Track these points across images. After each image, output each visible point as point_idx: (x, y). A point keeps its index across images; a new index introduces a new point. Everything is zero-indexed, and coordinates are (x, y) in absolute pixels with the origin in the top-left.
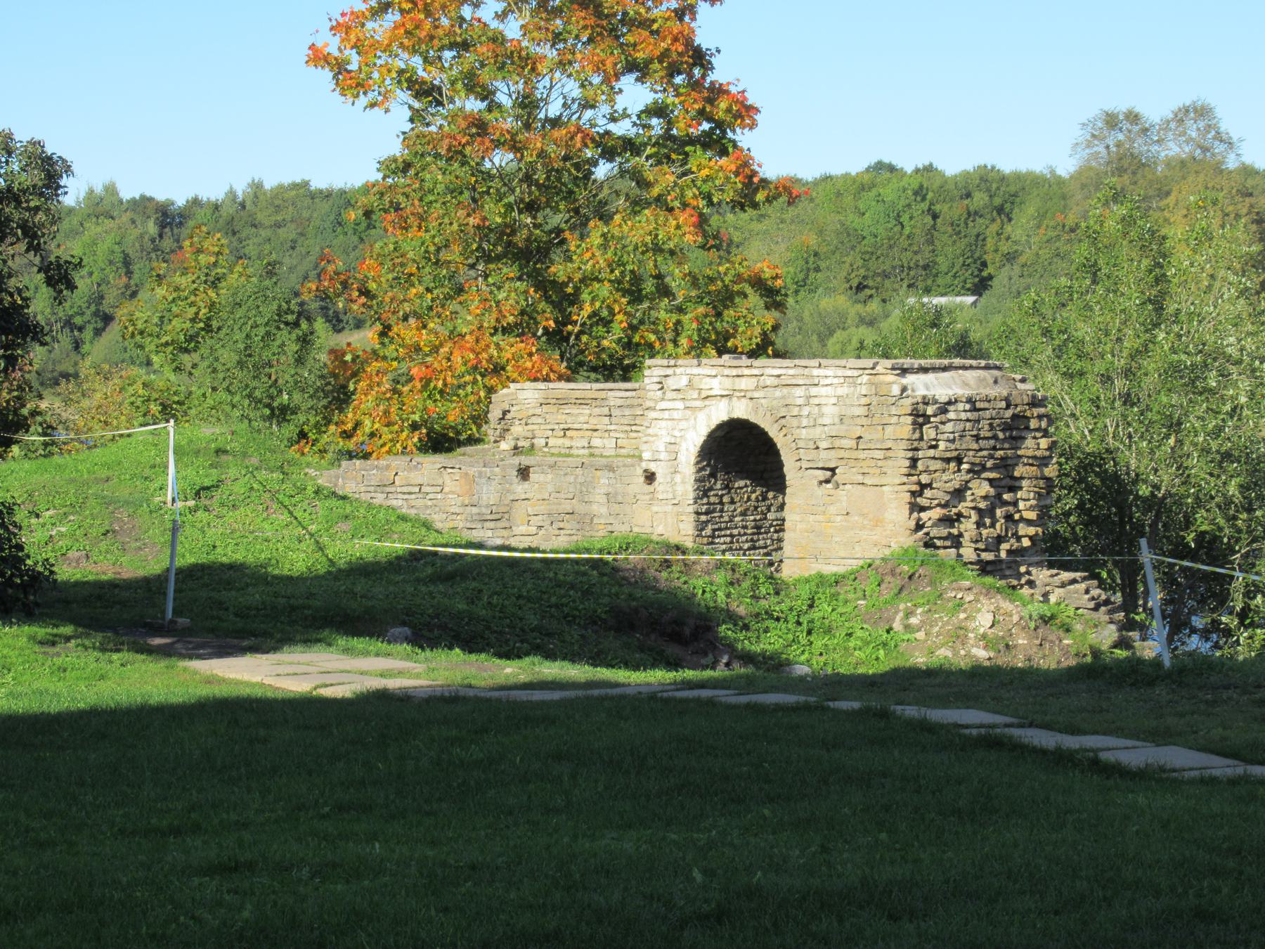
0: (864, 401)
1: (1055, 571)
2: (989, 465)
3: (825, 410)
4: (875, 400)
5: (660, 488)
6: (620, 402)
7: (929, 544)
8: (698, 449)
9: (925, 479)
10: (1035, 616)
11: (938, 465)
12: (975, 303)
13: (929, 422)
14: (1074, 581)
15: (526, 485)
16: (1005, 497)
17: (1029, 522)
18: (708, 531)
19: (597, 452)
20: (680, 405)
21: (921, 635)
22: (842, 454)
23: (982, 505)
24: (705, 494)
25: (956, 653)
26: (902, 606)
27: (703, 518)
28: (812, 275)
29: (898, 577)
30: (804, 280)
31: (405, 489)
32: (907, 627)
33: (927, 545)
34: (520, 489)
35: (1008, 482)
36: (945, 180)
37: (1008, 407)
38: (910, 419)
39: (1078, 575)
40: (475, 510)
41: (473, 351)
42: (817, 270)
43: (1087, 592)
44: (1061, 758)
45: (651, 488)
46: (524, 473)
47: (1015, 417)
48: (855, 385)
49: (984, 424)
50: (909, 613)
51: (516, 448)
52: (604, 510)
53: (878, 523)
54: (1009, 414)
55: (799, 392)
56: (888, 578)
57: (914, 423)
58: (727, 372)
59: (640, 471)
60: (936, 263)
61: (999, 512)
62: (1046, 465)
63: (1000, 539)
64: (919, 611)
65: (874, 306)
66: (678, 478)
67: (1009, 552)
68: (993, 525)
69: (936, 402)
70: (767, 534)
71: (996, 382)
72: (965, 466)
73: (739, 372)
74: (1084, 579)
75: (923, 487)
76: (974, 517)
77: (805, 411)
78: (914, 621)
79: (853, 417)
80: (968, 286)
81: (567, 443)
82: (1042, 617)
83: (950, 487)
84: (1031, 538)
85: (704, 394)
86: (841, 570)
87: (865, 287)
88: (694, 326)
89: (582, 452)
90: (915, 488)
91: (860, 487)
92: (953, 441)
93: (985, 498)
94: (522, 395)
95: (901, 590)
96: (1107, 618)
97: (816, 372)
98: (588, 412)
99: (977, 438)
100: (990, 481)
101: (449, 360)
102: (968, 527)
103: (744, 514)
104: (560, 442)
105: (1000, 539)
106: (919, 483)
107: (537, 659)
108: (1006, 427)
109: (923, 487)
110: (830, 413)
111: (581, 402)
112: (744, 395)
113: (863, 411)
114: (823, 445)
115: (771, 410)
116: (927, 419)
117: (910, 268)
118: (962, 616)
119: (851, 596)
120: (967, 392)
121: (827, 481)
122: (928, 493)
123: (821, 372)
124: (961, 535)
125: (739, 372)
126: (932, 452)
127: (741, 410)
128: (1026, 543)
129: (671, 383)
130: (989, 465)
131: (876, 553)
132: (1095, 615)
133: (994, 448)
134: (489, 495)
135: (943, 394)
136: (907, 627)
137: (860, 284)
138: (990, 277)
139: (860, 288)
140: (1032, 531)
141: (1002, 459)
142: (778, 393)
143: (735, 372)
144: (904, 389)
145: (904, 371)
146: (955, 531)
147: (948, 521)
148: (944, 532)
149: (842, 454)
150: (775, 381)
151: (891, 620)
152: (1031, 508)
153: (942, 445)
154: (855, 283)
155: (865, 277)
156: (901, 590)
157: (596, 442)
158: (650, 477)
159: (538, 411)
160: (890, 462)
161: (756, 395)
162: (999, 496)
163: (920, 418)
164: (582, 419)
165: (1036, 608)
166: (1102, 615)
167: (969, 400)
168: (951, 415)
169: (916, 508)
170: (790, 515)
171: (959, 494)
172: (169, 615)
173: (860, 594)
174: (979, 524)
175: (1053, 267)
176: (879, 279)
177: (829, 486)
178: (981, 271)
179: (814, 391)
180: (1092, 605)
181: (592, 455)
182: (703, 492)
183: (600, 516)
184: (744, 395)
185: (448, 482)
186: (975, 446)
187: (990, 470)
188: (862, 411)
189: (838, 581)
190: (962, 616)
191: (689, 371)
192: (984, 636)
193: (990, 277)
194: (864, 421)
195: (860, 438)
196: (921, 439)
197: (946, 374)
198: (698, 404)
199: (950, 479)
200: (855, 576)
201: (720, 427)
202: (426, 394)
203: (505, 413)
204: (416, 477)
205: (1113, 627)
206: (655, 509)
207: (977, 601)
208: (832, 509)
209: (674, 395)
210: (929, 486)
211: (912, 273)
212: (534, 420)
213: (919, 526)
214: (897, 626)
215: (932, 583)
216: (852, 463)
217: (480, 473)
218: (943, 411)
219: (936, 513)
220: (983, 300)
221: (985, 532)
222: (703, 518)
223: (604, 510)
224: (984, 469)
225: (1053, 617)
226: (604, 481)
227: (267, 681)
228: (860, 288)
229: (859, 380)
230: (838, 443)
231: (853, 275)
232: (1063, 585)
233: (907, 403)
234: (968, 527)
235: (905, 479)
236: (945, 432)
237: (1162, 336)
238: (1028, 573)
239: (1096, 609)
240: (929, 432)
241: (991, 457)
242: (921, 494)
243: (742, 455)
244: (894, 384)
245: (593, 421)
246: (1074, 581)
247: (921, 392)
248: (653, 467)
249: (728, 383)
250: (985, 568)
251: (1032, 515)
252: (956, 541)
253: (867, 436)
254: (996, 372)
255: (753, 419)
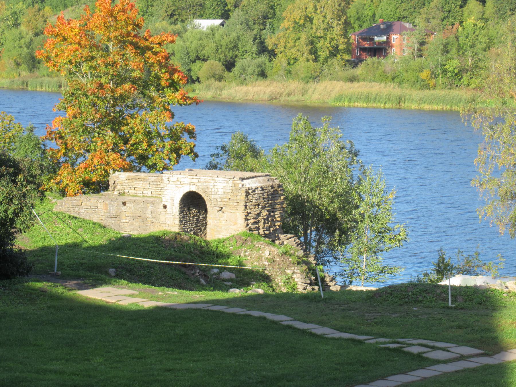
0: (231, 188)
1: (285, 235)
2: (267, 206)
3: (219, 190)
5: (168, 210)
6: (152, 180)
7: (250, 230)
8: (180, 199)
9: (249, 211)
10: (281, 252)
11: (253, 207)
12: (222, 25)
14: (291, 238)
15: (125, 207)
16: (272, 214)
17: (278, 221)
18: (183, 223)
19: (145, 195)
20: (174, 186)
21: (249, 258)
22: (224, 203)
23: (265, 217)
24: (182, 212)
25: (259, 264)
26: (243, 249)
27: (182, 219)
28: (150, 8)
29: (243, 240)
30: (146, 10)
31: (85, 207)
32: (245, 255)
33: (250, 231)
34: (123, 208)
35: (272, 210)
37: (272, 188)
38: (245, 194)
39: (292, 235)
40: (108, 214)
41: (100, 158)
42: (152, 6)
43: (295, 241)
44: (304, 332)
45: (165, 210)
46: (124, 204)
47: (274, 191)
49: (266, 194)
50: (246, 251)
51: (119, 193)
52: (150, 216)
53: (235, 224)
54: (272, 190)
55: (211, 184)
56: (239, 240)
57: (246, 195)
58: (189, 177)
59: (162, 205)
60: (205, 4)
61: (270, 219)
62: (283, 204)
63: (270, 227)
64: (248, 250)
65: (179, 26)
66: (174, 207)
67: (273, 230)
68: (268, 223)
69: (252, 189)
70: (201, 225)
71: (268, 180)
72: (260, 207)
73: (193, 177)
74: (294, 237)
75: (248, 213)
76: (263, 221)
77: (213, 190)
78: (247, 254)
80: (220, 14)
81: (135, 192)
82: (283, 252)
83: (256, 213)
84: (279, 226)
85: (182, 183)
86: (225, 237)
87: (175, 15)
88: (169, 147)
89: (140, 195)
90: (246, 214)
92: (257, 200)
93: (266, 215)
94: (120, 177)
95: (243, 244)
96: (300, 248)
97: (216, 179)
98: (142, 182)
99: (263, 198)
100: (267, 210)
101: (92, 160)
102: (261, 224)
103: (193, 217)
104: (133, 191)
105: (270, 227)
106: (247, 213)
107: (164, 288)
108: (271, 194)
109: (248, 213)
110: (221, 191)
111: (139, 179)
112: (194, 184)
114: (219, 200)
115: (203, 189)
116: (249, 194)
117: (193, 6)
118: (261, 252)
119: (228, 246)
120: (260, 185)
121: (220, 211)
122: (250, 215)
123: (218, 179)
124: (259, 227)
125: (193, 177)
126: (251, 203)
127: (194, 189)
128: (277, 227)
129: (171, 179)
130: (267, 206)
131: (235, 233)
132: (297, 248)
133: (268, 201)
134: (113, 210)
135: (254, 186)
136: (245, 255)
137: (172, 13)
139: (172, 15)
140: (279, 223)
141: (271, 203)
142: (205, 184)
143: (191, 177)
144: (243, 185)
145: (242, 179)
146: (257, 226)
147: (256, 223)
148: (255, 226)
149: (224, 203)
150: (204, 181)
151: (240, 253)
152: (279, 217)
153: (254, 201)
154: (170, 13)
155: (174, 10)
156: (243, 244)
157: (145, 192)
158: (165, 207)
159: (126, 182)
161: (198, 184)
162: (270, 214)
163: (247, 194)
164: (140, 185)
165: (282, 250)
166: (299, 248)
167: (262, 187)
168: (256, 192)
169: (247, 220)
170: (209, 221)
171: (259, 215)
172: (56, 271)
173: (231, 245)
174: (264, 223)
175: (256, 7)
176: (180, 11)
177: (221, 212)
178: (224, 7)
179: (215, 184)
180: (296, 245)
181: (143, 196)
182: (182, 211)
183: (149, 218)
184: (194, 184)
185: (99, 205)
186: (263, 201)
187: (267, 207)
188: (230, 191)
189: (224, 241)
190: (261, 252)
191: (177, 176)
192: (267, 258)
194: (231, 194)
196: (248, 200)
198: (180, 186)
199: (256, 211)
200: (229, 239)
201: (187, 193)
202: (85, 172)
203: (115, 182)
204: (89, 203)
205: (302, 251)
206: (167, 216)
207: (265, 247)
208: (222, 219)
209: (172, 183)
210: (250, 213)
211: (194, 8)
212: (124, 184)
213: (248, 225)
214: (242, 255)
215: (252, 242)
217: (110, 203)
218: (254, 191)
219: (252, 221)
220: (227, 22)
221: (266, 225)
222: (182, 219)
223: (150, 216)
224: (265, 207)
225: (287, 252)
226: (150, 207)
227: (103, 299)
228: (172, 15)
231: (169, 9)
232: (288, 239)
233: (244, 189)
234: (261, 224)
236: (254, 198)
237: (315, 161)
238: (278, 236)
239: (297, 246)
240: (250, 197)
241: (268, 203)
242: (248, 215)
243: (193, 202)
244: (240, 183)
245: (144, 185)
246: (291, 238)
247: (248, 186)
248: (166, 204)
249: (189, 180)
250: (266, 236)
251: (279, 219)
252: (258, 229)
253: (232, 198)
254: (268, 177)
255: (197, 191)
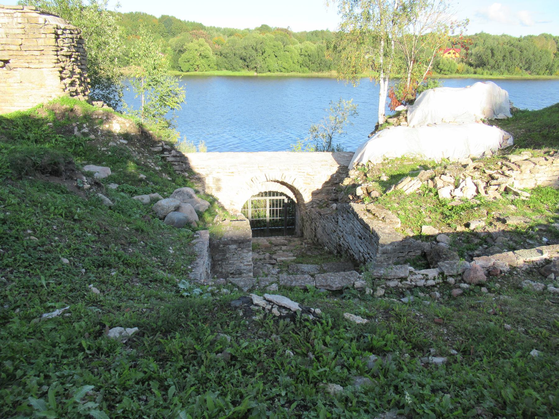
4: (28, 26)
13: (59, 38)
22: (11, 53)
36: (330, 32)
48: (13, 17)
79: (15, 34)
91: (27, 69)
113: (21, 31)
138: (420, 166)
149: (11, 53)
160: (45, 57)
169: (62, 79)
193: (420, 166)
194: (23, 36)
195: (21, 45)
197: (285, 181)
216: (20, 58)
229: (15, 15)
230: (7, 47)
235: (54, 65)
